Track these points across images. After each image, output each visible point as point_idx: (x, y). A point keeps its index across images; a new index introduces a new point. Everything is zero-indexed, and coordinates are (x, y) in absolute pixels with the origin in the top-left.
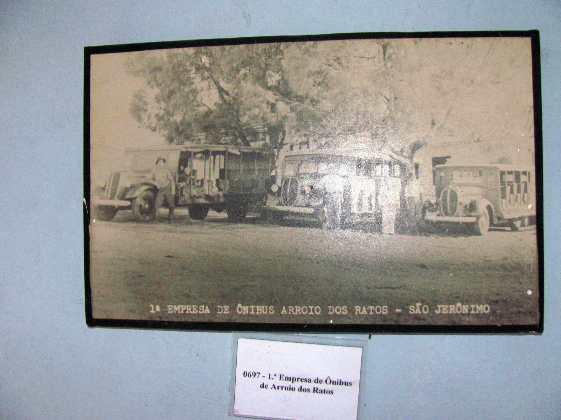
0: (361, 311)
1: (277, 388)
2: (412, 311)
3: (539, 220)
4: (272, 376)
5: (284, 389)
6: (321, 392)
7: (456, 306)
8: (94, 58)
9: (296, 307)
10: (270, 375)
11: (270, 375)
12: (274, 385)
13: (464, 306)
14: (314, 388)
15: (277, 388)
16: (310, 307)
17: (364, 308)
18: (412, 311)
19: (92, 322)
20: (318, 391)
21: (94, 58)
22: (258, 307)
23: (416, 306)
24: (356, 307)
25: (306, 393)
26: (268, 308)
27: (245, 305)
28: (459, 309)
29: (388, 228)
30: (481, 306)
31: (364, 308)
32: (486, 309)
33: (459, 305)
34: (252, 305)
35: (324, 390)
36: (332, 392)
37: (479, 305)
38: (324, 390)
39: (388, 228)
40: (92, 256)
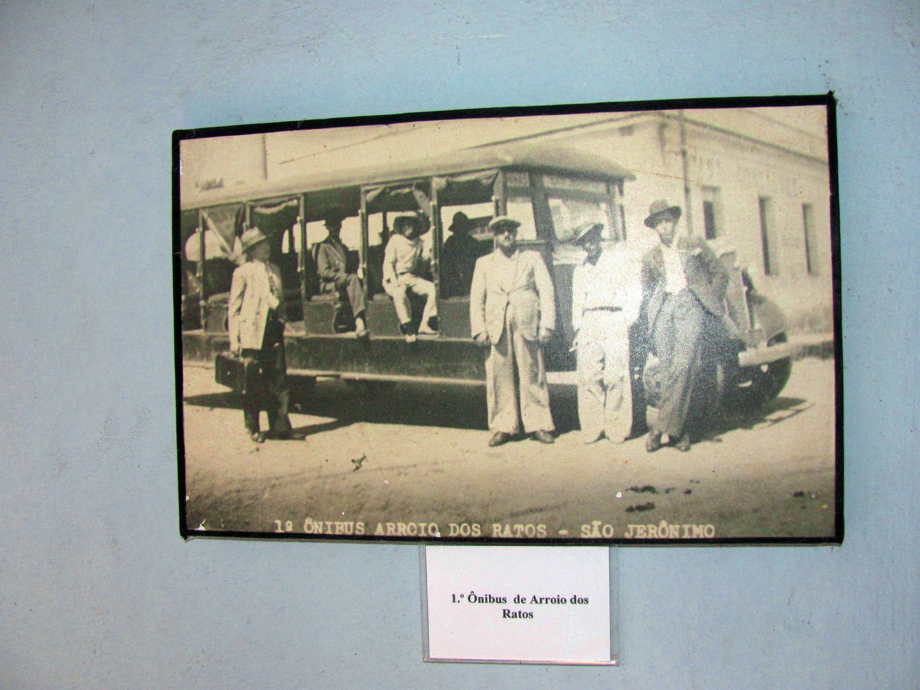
0: (502, 531)
1: (538, 601)
2: (586, 534)
3: (837, 350)
4: (458, 598)
5: (549, 601)
6: (515, 615)
7: (658, 526)
8: (184, 144)
9: (399, 524)
10: (454, 596)
11: (454, 596)
12: (534, 597)
13: (671, 527)
14: (504, 611)
15: (538, 601)
16: (327, 523)
17: (507, 527)
18: (586, 534)
19: (838, 537)
20: (511, 615)
21: (184, 144)
22: (337, 523)
23: (592, 526)
24: (495, 526)
25: (583, 605)
26: (354, 526)
27: (318, 520)
28: (663, 531)
29: (605, 412)
30: (701, 526)
31: (507, 527)
32: (710, 531)
33: (663, 524)
34: (328, 520)
35: (520, 613)
36: (531, 615)
37: (698, 525)
38: (520, 613)
39: (605, 412)
40: (188, 461)
